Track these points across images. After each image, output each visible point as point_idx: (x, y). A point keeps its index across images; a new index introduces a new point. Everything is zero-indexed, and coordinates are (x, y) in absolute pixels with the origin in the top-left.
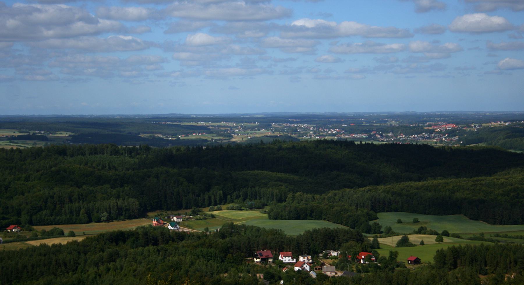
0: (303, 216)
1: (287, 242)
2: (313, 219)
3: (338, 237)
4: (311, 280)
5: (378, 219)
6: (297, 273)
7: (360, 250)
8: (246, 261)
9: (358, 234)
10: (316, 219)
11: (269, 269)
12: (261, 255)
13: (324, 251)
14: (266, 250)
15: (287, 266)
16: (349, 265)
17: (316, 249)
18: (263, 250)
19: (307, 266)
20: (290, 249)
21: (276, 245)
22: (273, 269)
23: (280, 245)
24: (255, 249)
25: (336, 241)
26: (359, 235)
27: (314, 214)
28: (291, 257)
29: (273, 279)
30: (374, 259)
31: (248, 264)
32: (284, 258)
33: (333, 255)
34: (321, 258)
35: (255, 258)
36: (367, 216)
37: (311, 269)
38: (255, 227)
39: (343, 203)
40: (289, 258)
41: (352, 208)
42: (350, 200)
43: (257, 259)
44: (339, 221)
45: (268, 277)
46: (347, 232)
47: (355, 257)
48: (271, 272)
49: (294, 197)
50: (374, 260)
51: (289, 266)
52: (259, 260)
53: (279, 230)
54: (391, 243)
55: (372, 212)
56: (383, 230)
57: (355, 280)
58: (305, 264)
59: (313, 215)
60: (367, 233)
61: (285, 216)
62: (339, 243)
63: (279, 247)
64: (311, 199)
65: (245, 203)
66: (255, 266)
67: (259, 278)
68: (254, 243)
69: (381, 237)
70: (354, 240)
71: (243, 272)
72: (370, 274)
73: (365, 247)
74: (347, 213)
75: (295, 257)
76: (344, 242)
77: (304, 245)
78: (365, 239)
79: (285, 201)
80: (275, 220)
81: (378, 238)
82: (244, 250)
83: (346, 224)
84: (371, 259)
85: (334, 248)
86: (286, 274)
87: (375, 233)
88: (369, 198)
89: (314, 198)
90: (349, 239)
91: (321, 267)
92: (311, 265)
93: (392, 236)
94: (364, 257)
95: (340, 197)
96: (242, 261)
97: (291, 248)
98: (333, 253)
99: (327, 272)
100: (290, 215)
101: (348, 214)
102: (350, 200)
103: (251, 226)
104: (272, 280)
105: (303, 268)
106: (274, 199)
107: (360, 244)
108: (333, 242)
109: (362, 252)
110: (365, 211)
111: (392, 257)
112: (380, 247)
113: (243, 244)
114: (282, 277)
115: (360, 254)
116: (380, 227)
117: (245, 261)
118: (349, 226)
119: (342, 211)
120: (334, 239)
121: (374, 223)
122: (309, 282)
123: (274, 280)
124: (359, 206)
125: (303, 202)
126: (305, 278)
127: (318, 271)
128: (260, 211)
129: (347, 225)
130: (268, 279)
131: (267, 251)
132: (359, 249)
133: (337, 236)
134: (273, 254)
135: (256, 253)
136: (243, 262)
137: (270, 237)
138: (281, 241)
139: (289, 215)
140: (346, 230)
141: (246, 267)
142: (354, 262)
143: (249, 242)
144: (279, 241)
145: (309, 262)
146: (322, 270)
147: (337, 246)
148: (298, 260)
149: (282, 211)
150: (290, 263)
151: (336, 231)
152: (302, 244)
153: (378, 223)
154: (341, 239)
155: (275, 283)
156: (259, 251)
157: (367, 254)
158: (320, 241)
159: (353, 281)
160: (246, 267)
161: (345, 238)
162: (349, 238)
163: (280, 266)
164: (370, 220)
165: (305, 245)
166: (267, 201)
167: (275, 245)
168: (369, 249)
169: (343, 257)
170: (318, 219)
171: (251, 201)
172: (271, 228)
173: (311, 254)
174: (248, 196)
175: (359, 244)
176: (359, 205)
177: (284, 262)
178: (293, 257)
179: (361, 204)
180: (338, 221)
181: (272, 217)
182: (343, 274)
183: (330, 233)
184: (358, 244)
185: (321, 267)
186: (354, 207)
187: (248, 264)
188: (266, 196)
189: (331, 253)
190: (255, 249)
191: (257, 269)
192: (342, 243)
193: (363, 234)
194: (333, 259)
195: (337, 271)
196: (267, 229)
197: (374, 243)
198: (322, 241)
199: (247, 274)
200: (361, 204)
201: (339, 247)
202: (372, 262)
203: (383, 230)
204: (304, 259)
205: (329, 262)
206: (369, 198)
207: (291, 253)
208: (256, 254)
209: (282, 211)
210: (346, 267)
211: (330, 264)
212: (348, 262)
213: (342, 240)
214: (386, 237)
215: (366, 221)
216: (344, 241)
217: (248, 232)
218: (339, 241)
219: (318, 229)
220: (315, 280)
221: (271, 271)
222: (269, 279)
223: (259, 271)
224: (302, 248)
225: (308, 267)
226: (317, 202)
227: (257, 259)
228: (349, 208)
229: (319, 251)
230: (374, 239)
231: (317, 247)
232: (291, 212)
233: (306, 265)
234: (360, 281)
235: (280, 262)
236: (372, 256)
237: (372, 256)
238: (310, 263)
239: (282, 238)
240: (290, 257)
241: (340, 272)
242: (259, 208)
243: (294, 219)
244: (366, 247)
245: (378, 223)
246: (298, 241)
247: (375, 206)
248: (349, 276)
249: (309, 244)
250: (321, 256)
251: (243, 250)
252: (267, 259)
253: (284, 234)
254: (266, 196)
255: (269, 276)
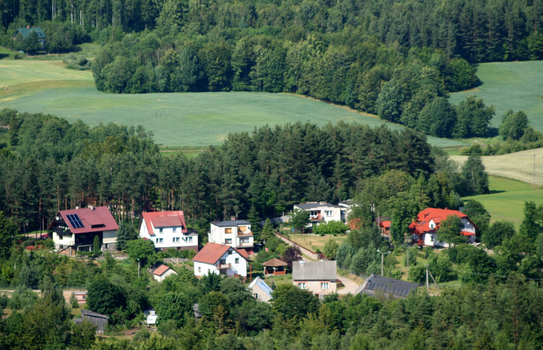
0: (217, 78)
1: (167, 175)
2: (252, 87)
3: (345, 156)
4: (253, 310)
5: (480, 87)
6: (203, 285)
7: (421, 201)
8: (22, 245)
9: (414, 146)
10: (261, 88)
11: (105, 273)
12: (76, 221)
13: (297, 204)
14: (92, 204)
15: (166, 260)
16: (385, 256)
17: (267, 198)
18: (83, 205)
19: (237, 260)
20: (177, 199)
21: (127, 189)
22: (119, 271)
23: (142, 187)
24: (53, 200)
25: (336, 170)
26: (418, 146)
27: (257, 71)
28: (183, 228)
29: (121, 307)
30: (472, 231)
31: (32, 253)
32: (156, 231)
33: (328, 219)
34: (285, 228)
35: (55, 234)
36: (440, 75)
37: (252, 270)
38: (49, 117)
39: (356, 32)
40: (174, 230)
41: (389, 49)
42: (382, 19)
43: (61, 238)
44: (345, 96)
45: (103, 302)
46: (377, 138)
47: (404, 226)
48: (115, 284)
49: (184, 10)
50: (469, 236)
51: (176, 261)
52: (69, 241)
53: (133, 127)
54: (530, 174)
55: (459, 61)
56: (495, 123)
57: (409, 313)
58: (230, 253)
59: (251, 74)
60: (441, 137)
61: (154, 80)
62: (347, 175)
63: (137, 194)
64: (246, 17)
65: (10, 31)
66: (56, 261)
67: (71, 306)
68: (50, 181)
69: (491, 152)
70: (400, 164)
71: (15, 284)
72: (457, 285)
73: (440, 191)
74: (373, 64)
75: (196, 227)
76: (366, 172)
77: (228, 185)
78: (438, 160)
79: (152, 24)
80: (120, 93)
81: (481, 155)
82: (17, 205)
83: (367, 107)
84: (459, 231)
85: (331, 193)
86: (167, 290)
87: (469, 134)
88: (447, 13)
89: (255, 15)
90: (382, 163)
91: (285, 264)
92: (253, 256)
93: (532, 147)
94: (437, 224)
95: (348, 10)
96: (9, 243)
97: (183, 196)
98: (327, 212)
99: (309, 282)
100: (172, 76)
101: (377, 68)
102: (382, 19)
103: (35, 116)
104: (119, 312)
105: (223, 266)
106: (114, 20)
107: (421, 179)
108: (327, 173)
109: (429, 210)
110: (435, 57)
111: (533, 223)
112: (491, 189)
113: (13, 186)
114: (151, 300)
115: (421, 215)
116: (488, 115)
117: (18, 243)
118: (380, 112)
119: (354, 60)
120: (330, 163)
121: (468, 99)
122: (246, 317)
123: (123, 311)
124: (412, 43)
125: (218, 28)
126: (233, 304)
127: (280, 279)
128: (65, 62)
129: (370, 109)
130: (102, 310)
131: (99, 209)
132: (418, 198)
133: (342, 154)
134: (117, 219)
135: (59, 215)
136: (14, 249)
137: (106, 158)
138: (146, 173)
139: (169, 78)
140: (370, 130)
141: (24, 264)
142: (402, 242)
143: (34, 180)
144: (138, 175)
145: (245, 245)
146: (289, 271)
147: (340, 188)
148: (205, 239)
149: (143, 63)
150: (179, 248)
151: (338, 134)
152: (219, 182)
153: (481, 101)
154: (353, 164)
155: (126, 321)
156: (69, 208)
157: (446, 214)
158: (282, 170)
159: (403, 316)
160: (24, 264)
161: (370, 158)
162: (382, 160)
163: (143, 262)
164: (452, 91)
165: (232, 185)
166: (90, 24)
167: (127, 185)
168: (454, 197)
169: (364, 226)
170: (270, 90)
171: (32, 24)
172: (106, 124)
173: (250, 215)
174: (22, 7)
175: (417, 178)
176: (412, 39)
177: (157, 245)
178: (188, 229)
179: (421, 35)
180: (338, 94)
181: (107, 84)
182: (366, 288)
183: (315, 144)
184: (413, 179)
185: (285, 264)
186: (394, 46)
187: (32, 258)
188: (85, 6)
189: (319, 212)
190: (53, 200)
191: (63, 271)
192: (360, 179)
193: (433, 141)
194: (328, 232)
195: (343, 275)
196: (92, 127)
197: (470, 173)
198: (290, 172)
199: (29, 290)
200: (421, 35)
201: (347, 191)
202: (462, 241)
203: (495, 123)
204: (228, 236)
205: (313, 244)
206: (447, 13)
207: (181, 213)
208: (57, 218)
209: (143, 63)
210: (374, 262)
211: (318, 252)
212: (380, 242)
213: (360, 167)
214: (509, 152)
215: (440, 94)
216: (364, 170)
217: (23, 136)
218: (348, 168)
219: (273, 129)
220: (267, 311)
221: (114, 279)
222: (106, 306)
223: (69, 280)
224: (220, 196)
225: (243, 263)
226: (266, 27)
227: (61, 238)
228: (379, 50)
229: (278, 207)
230: (469, 162)
231: (273, 192)
232: (177, 63)
233: (235, 255)
234: (427, 316)
235: (143, 247)
236: (464, 221)
237: (464, 221)
238: (248, 249)
239: (148, 163)
240: (179, 230)
241: (355, 279)
242: (60, 49)
243: (186, 88)
244: (444, 189)
245: (481, 101)
246: (206, 171)
247: (470, 41)
248: (387, 295)
249: (245, 183)
250: (286, 225)
251: (11, 206)
252: (96, 238)
253: (151, 142)
254: (85, 6)
255: (106, 297)
